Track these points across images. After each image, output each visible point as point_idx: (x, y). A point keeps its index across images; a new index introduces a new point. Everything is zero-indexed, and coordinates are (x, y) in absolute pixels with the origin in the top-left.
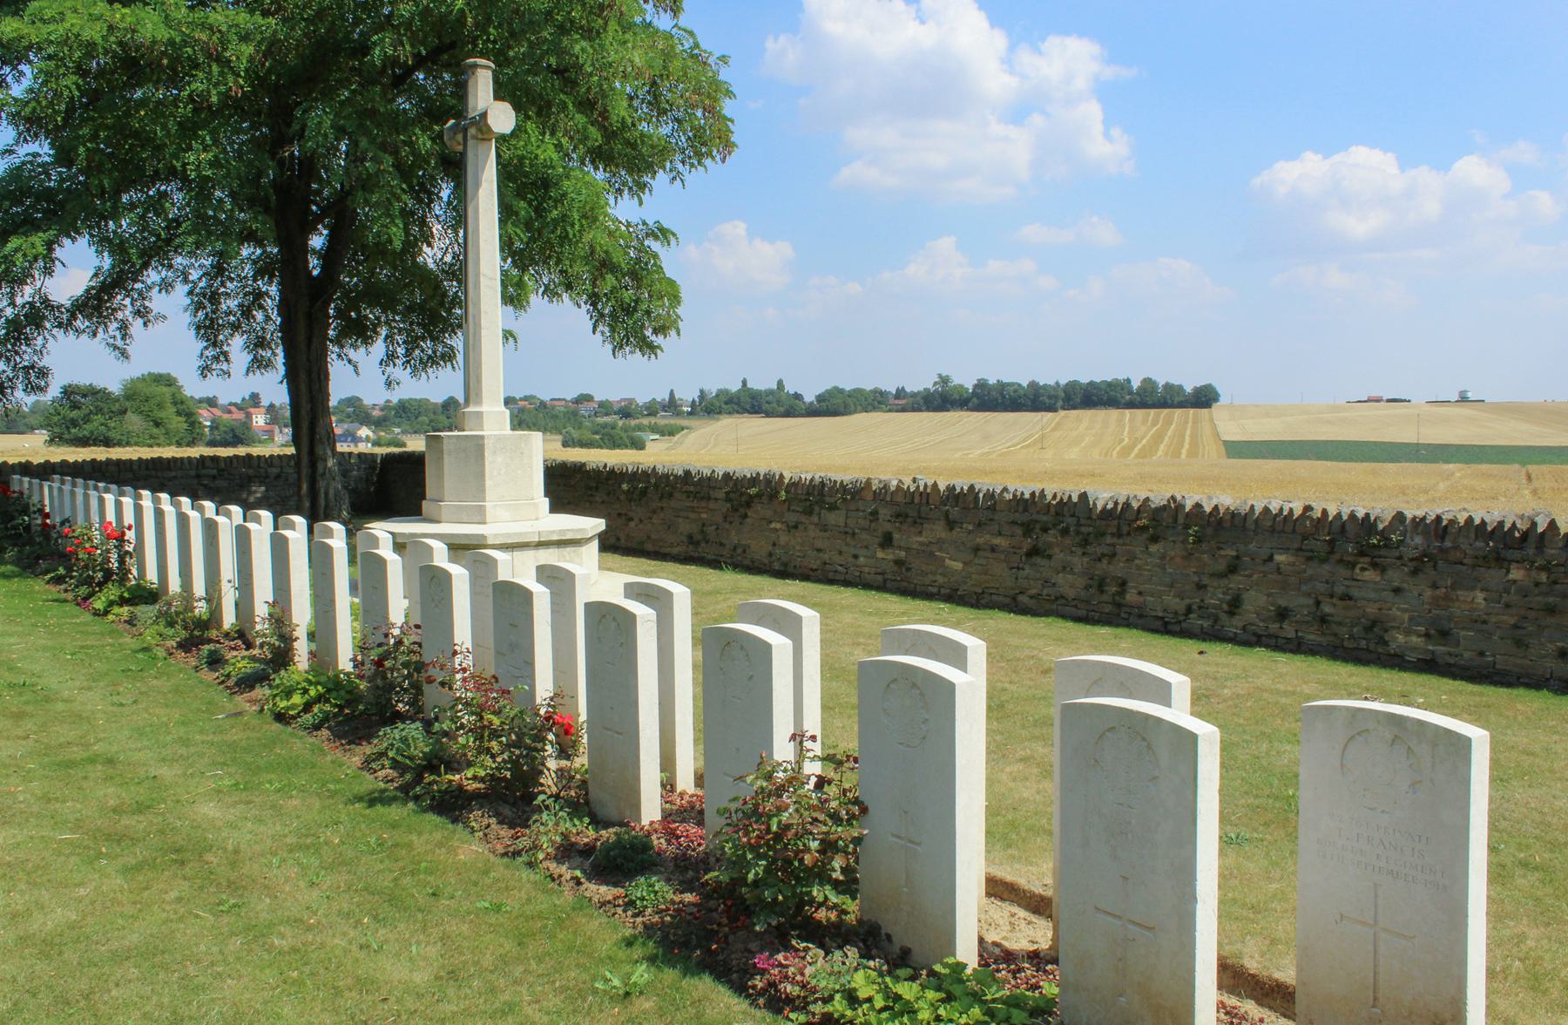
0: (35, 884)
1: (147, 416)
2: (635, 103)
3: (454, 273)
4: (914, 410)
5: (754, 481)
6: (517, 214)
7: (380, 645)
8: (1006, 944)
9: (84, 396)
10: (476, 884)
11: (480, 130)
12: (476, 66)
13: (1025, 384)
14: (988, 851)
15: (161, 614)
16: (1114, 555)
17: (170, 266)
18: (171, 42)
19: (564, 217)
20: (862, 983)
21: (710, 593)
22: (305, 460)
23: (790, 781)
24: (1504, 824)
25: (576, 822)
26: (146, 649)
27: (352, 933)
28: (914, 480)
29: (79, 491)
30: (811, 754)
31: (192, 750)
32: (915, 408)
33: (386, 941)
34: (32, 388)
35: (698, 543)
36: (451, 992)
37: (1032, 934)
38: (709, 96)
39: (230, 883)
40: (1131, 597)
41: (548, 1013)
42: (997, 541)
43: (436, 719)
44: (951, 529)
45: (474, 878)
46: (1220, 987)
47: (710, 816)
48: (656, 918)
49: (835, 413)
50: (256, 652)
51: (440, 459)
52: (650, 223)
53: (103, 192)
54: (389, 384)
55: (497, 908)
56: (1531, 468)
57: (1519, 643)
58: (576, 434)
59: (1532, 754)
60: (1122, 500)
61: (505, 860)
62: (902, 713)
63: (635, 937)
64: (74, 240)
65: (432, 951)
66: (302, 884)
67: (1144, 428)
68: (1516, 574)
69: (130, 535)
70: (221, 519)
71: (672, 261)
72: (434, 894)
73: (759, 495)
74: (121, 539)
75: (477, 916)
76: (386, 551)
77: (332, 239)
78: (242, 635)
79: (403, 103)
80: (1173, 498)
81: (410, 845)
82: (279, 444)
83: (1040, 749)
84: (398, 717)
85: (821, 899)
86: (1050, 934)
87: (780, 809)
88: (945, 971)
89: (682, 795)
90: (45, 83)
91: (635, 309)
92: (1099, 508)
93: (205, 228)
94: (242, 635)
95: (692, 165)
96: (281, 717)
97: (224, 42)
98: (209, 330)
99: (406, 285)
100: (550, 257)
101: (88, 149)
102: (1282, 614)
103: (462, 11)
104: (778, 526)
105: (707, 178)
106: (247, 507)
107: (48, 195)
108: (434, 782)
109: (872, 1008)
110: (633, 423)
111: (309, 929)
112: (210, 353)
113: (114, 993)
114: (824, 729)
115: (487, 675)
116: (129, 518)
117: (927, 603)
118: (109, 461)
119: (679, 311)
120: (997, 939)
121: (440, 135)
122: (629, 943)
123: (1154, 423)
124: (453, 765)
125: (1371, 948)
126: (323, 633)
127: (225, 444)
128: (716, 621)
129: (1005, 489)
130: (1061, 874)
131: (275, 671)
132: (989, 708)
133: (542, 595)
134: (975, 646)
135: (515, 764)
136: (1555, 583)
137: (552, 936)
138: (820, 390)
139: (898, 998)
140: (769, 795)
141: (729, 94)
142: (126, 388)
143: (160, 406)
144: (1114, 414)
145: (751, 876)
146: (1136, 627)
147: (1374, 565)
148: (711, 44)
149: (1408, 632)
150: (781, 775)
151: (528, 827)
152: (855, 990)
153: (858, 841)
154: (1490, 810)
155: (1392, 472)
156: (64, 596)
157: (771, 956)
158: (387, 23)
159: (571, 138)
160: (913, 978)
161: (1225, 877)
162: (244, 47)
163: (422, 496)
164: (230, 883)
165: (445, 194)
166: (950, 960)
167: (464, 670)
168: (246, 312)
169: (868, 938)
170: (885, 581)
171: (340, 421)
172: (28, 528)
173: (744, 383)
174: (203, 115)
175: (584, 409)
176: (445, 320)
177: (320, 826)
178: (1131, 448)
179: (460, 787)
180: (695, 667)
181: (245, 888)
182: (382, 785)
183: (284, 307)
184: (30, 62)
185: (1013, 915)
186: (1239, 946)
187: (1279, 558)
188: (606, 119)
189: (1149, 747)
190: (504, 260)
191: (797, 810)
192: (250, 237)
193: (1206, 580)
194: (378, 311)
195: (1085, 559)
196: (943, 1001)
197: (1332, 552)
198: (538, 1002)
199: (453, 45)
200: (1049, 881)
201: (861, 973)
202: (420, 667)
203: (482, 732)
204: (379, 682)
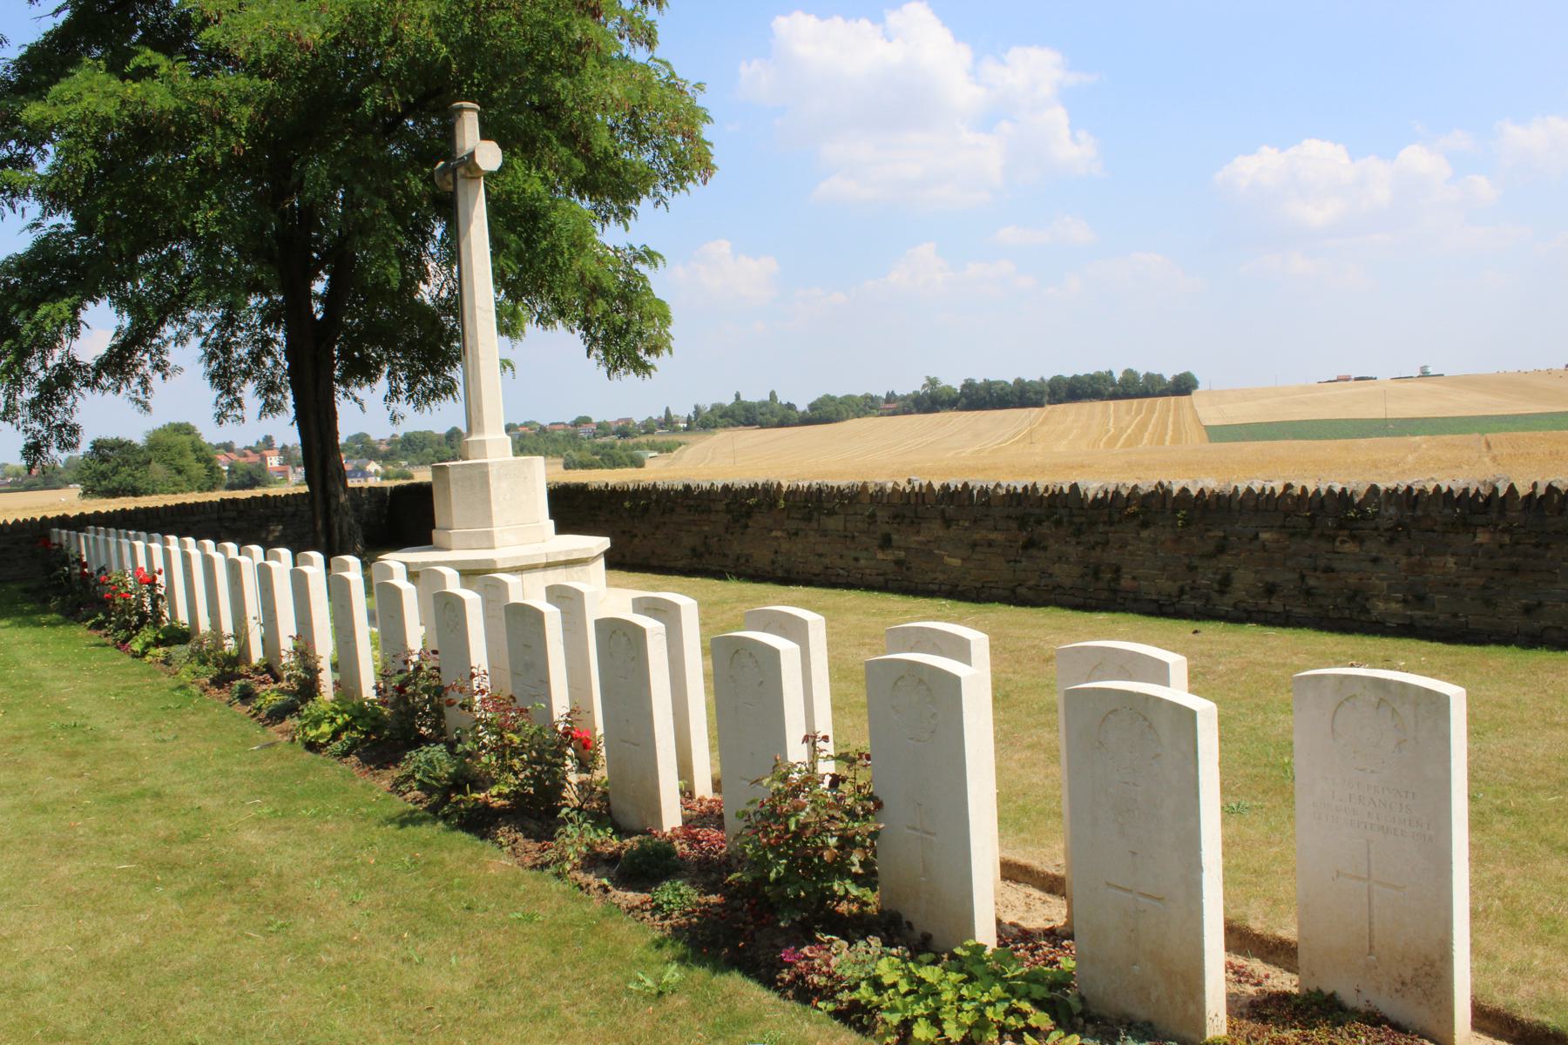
0: (100, 911)
1: (169, 464)
2: (616, 133)
3: (450, 308)
4: (905, 413)
5: (753, 491)
6: (508, 247)
7: (400, 672)
8: (1024, 924)
9: (112, 449)
10: (508, 897)
11: (469, 169)
12: (462, 109)
13: (1011, 382)
14: (1001, 837)
15: (193, 653)
16: (1107, 542)
17: (184, 321)
18: (178, 110)
19: (553, 247)
20: (887, 970)
21: (716, 604)
22: (318, 495)
23: (805, 781)
24: (1482, 774)
25: (600, 832)
26: (182, 687)
27: (394, 948)
28: (909, 482)
29: (113, 540)
30: (824, 754)
31: (231, 780)
32: (906, 411)
33: (427, 954)
34: (66, 445)
35: (701, 556)
36: (491, 999)
37: (1045, 913)
38: (687, 122)
39: (277, 905)
40: (1126, 582)
41: (585, 1015)
42: (993, 536)
43: (459, 740)
44: (948, 527)
45: (506, 891)
46: (1228, 949)
47: (729, 820)
48: (683, 921)
49: (828, 421)
50: (284, 684)
51: (447, 488)
52: (637, 247)
53: (121, 256)
54: (394, 419)
55: (530, 919)
56: (1489, 436)
57: (1488, 602)
58: (576, 456)
59: (1505, 706)
60: (1111, 489)
61: (534, 872)
62: (913, 709)
63: (664, 939)
64: (96, 302)
65: (471, 962)
66: (343, 903)
67: (1128, 418)
68: (1482, 538)
69: (161, 579)
70: (243, 559)
71: (659, 283)
72: (468, 908)
73: (758, 505)
74: (152, 583)
75: (511, 927)
76: (400, 580)
77: (332, 283)
78: (270, 669)
79: (395, 150)
80: (1160, 484)
81: (442, 863)
82: (293, 483)
83: (1046, 735)
84: (421, 741)
85: (842, 893)
86: (1064, 912)
87: (798, 809)
88: (967, 953)
89: (700, 801)
90: (66, 159)
91: (627, 332)
92: (1090, 497)
93: (222, 287)
94: (270, 669)
95: (675, 189)
96: (312, 746)
97: (226, 107)
98: (223, 379)
99: (406, 322)
100: (542, 286)
101: (106, 217)
102: (1270, 590)
103: (446, 58)
104: (779, 534)
105: (689, 200)
106: (267, 546)
107: (72, 262)
108: (461, 801)
109: (898, 993)
110: (631, 442)
111: (353, 945)
112: (225, 400)
113: (180, 1010)
114: (835, 729)
115: (506, 694)
116: (159, 563)
117: (928, 601)
118: (137, 509)
119: (670, 330)
120: (1014, 919)
121: (431, 177)
122: (659, 945)
123: (1138, 412)
124: (480, 783)
125: (1365, 900)
126: (345, 663)
127: (243, 487)
128: (724, 630)
129: (998, 485)
130: (1071, 853)
131: (304, 702)
132: (995, 699)
133: (553, 617)
134: (979, 641)
135: (537, 779)
136: (1517, 543)
137: (584, 943)
138: (813, 398)
139: (921, 981)
140: (786, 797)
141: (707, 119)
142: (149, 439)
143: (181, 454)
144: (1098, 406)
145: (773, 875)
146: (1132, 611)
147: (1353, 537)
148: (686, 72)
149: (1387, 600)
150: (796, 776)
151: (554, 839)
152: (880, 977)
153: (874, 835)
154: (1469, 763)
155: (1364, 447)
156: (104, 640)
157: (797, 949)
158: (375, 76)
159: (556, 171)
160: (935, 963)
161: (1228, 845)
162: (244, 109)
163: (432, 526)
164: (277, 905)
165: (438, 233)
166: (970, 943)
167: (482, 692)
168: (256, 359)
169: (891, 927)
170: (887, 581)
171: (350, 458)
172: (68, 577)
173: (738, 396)
174: (209, 174)
175: (582, 432)
176: (444, 354)
177: (355, 848)
178: (1116, 438)
179: (486, 805)
180: (705, 676)
181: (291, 909)
182: (411, 806)
183: (290, 352)
184: (53, 141)
185: (1028, 896)
186: (1244, 909)
187: (1264, 536)
188: (589, 150)
189: (1150, 726)
190: (498, 292)
191: (814, 809)
192: (256, 287)
193: (1196, 562)
194: (380, 350)
195: (1080, 548)
196: (965, 981)
197: (1313, 527)
198: (574, 1005)
199: (439, 91)
200: (1061, 861)
201: (885, 960)
202: (440, 691)
203: (503, 750)
204: (402, 707)
